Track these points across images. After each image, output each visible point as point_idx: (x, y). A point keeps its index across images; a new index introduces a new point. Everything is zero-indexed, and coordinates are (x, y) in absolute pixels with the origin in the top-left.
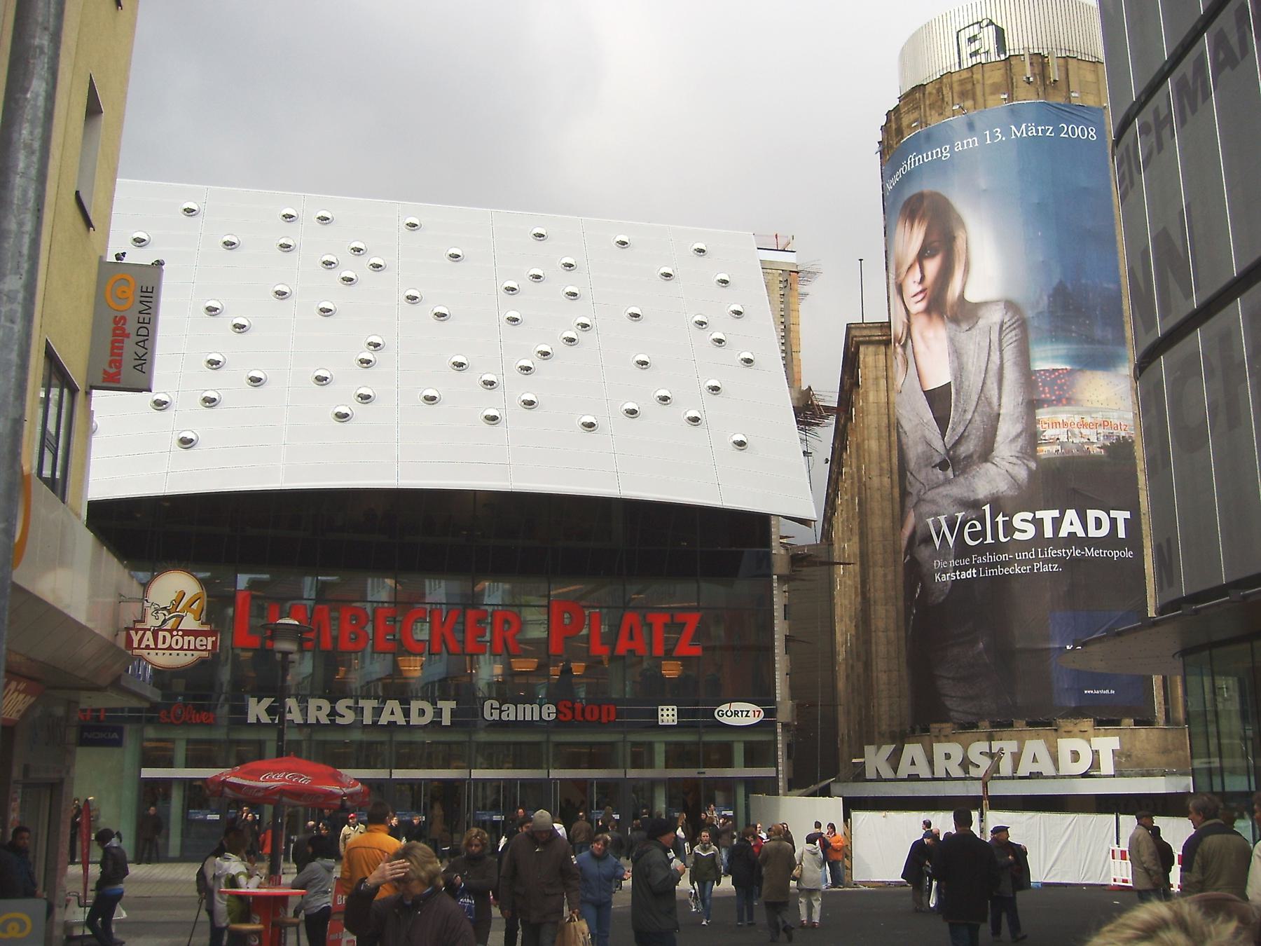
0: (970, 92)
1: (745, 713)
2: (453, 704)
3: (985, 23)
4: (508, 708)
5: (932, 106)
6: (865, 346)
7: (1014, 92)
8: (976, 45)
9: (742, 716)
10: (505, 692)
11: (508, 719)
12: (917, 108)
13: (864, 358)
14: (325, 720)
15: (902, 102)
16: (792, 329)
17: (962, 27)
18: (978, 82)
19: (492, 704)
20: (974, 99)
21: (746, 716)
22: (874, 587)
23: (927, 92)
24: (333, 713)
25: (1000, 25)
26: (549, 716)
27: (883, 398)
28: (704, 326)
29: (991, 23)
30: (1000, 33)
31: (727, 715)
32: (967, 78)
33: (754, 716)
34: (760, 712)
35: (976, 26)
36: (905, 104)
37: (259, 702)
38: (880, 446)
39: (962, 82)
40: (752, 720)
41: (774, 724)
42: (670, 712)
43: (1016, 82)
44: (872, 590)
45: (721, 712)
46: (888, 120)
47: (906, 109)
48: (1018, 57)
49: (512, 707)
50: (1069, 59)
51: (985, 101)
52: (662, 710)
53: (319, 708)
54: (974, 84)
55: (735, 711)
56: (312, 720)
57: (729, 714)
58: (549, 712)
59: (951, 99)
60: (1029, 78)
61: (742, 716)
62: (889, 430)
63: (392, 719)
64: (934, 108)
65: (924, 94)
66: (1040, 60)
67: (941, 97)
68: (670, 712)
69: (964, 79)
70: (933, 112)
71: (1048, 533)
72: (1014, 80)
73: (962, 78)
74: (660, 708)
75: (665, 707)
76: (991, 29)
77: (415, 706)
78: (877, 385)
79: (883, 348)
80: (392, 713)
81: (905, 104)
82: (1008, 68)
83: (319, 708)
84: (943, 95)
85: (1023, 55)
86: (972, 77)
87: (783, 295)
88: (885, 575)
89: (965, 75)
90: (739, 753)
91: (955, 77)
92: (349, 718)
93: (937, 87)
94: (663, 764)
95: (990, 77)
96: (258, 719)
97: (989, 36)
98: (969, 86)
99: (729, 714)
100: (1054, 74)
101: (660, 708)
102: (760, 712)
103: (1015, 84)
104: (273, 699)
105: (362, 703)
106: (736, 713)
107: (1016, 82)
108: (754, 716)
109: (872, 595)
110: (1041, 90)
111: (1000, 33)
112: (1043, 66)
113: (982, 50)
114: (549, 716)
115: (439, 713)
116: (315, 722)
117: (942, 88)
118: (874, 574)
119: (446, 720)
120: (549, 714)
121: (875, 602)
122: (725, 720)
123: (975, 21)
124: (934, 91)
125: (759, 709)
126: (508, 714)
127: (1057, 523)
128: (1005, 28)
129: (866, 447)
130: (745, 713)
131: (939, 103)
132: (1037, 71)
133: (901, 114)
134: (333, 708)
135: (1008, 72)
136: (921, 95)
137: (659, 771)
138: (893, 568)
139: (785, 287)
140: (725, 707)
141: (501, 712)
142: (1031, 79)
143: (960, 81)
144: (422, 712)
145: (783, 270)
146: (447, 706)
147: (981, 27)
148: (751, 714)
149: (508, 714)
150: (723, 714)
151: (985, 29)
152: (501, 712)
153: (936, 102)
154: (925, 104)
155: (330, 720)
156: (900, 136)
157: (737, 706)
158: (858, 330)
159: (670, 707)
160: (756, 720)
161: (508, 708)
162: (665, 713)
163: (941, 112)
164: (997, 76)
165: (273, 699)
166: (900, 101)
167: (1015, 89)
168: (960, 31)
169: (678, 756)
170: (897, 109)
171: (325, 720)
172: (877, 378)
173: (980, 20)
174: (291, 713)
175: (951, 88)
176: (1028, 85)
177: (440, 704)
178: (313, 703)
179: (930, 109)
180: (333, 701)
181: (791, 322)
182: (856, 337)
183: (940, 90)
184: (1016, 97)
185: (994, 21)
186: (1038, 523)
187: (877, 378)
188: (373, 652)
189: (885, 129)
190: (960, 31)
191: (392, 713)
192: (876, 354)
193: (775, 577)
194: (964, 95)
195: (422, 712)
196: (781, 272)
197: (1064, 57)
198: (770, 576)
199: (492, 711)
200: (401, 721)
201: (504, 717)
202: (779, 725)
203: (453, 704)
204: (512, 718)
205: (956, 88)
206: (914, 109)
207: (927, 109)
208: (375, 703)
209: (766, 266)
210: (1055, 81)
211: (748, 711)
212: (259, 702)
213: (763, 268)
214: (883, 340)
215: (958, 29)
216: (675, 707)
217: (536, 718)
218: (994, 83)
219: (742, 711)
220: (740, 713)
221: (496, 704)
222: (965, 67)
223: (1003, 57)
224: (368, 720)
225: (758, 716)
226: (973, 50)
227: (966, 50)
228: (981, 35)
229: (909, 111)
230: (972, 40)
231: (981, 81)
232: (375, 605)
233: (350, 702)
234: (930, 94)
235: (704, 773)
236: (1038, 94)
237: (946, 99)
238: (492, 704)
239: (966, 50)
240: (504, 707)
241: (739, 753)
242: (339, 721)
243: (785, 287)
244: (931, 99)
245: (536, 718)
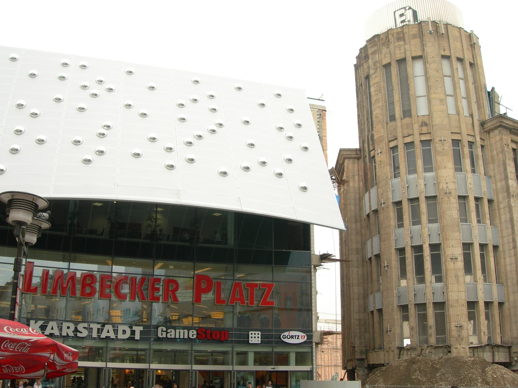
0: (402, 38)
1: (297, 337)
2: (141, 328)
3: (407, 8)
4: (171, 331)
5: (383, 44)
6: (348, 159)
7: (424, 38)
8: (403, 18)
9: (295, 338)
10: (168, 323)
11: (180, 330)
12: (376, 45)
13: (347, 165)
14: (71, 334)
15: (368, 43)
16: (323, 138)
17: (397, 10)
18: (406, 33)
19: (162, 329)
20: (404, 40)
21: (298, 338)
22: (352, 278)
23: (380, 38)
24: (76, 330)
25: (414, 9)
26: (193, 336)
27: (357, 185)
28: (282, 130)
29: (410, 8)
30: (415, 13)
31: (287, 338)
32: (401, 31)
33: (302, 338)
34: (305, 336)
35: (403, 9)
36: (370, 44)
37: (36, 323)
38: (355, 208)
39: (398, 33)
40: (301, 341)
41: (311, 343)
42: (257, 336)
43: (425, 33)
44: (351, 279)
45: (284, 336)
46: (360, 52)
47: (370, 46)
48: (425, 22)
49: (173, 331)
50: (448, 25)
51: (410, 42)
52: (258, 334)
53: (68, 328)
54: (404, 34)
55: (292, 336)
56: (64, 334)
57: (289, 337)
58: (193, 334)
59: (393, 40)
60: (431, 31)
61: (295, 338)
62: (360, 201)
63: (108, 335)
64: (384, 45)
65: (379, 39)
66: (435, 24)
67: (388, 40)
68: (257, 336)
69: (399, 32)
70: (384, 47)
71: (95, 335)
72: (424, 33)
73: (398, 31)
74: (250, 332)
75: (253, 332)
76: (411, 11)
77: (121, 328)
78: (354, 179)
79: (356, 160)
80: (108, 332)
81: (370, 44)
82: (420, 27)
83: (68, 328)
84: (389, 39)
85: (428, 21)
86: (403, 31)
87: (319, 121)
88: (358, 272)
89: (399, 30)
90: (292, 358)
91: (395, 31)
92: (85, 333)
93: (386, 35)
94: (409, 307)
95: (412, 31)
96: (67, 334)
97: (409, 15)
98: (401, 35)
99: (289, 337)
100: (443, 31)
101: (250, 332)
102: (305, 336)
103: (424, 34)
104: (44, 321)
105: (92, 326)
106: (292, 337)
107: (425, 33)
108: (302, 338)
109: (351, 281)
110: (436, 37)
111: (415, 13)
112: (436, 27)
113: (407, 20)
114: (193, 336)
115: (133, 332)
116: (66, 335)
117: (388, 35)
118: (352, 271)
119: (137, 337)
120: (193, 335)
121: (353, 285)
122: (286, 340)
123: (403, 7)
124: (384, 38)
125: (304, 335)
126: (171, 335)
127: (100, 331)
128: (417, 10)
129: (349, 208)
130: (297, 337)
131: (387, 43)
132: (434, 29)
133: (367, 48)
134: (76, 328)
135: (420, 29)
136: (378, 39)
137: (251, 367)
138: (362, 268)
139: (320, 117)
140: (286, 334)
141: (167, 333)
142: (432, 32)
143: (397, 32)
144: (124, 332)
145: (319, 109)
146: (138, 329)
147: (406, 10)
148: (300, 337)
149: (171, 335)
150: (285, 337)
151: (408, 11)
152: (167, 333)
153: (386, 42)
154: (380, 44)
155: (74, 334)
156: (367, 59)
157: (293, 333)
158: (345, 151)
159: (257, 333)
160: (303, 341)
161: (171, 331)
162: (253, 336)
163: (387, 47)
164: (415, 31)
165: (44, 321)
166: (367, 43)
167: (424, 37)
168: (396, 11)
169: (261, 359)
170: (366, 47)
171: (71, 334)
172: (354, 175)
173: (405, 7)
174: (53, 329)
175: (393, 36)
176: (430, 35)
177: (134, 328)
178: (65, 325)
179: (382, 46)
180: (76, 323)
181: (323, 135)
182: (343, 155)
183: (387, 37)
184: (425, 40)
185: (412, 7)
186: (90, 330)
187: (354, 175)
188: (80, 281)
189: (358, 58)
190: (396, 11)
191: (108, 332)
192: (354, 163)
193: (313, 266)
194: (399, 39)
195: (124, 332)
196: (318, 110)
197: (446, 24)
198: (310, 265)
199: (163, 332)
200: (112, 335)
201: (169, 336)
202: (314, 344)
203: (141, 328)
204: (173, 336)
205: (395, 36)
206: (375, 45)
207: (381, 46)
208: (99, 326)
209: (312, 107)
210: (443, 34)
211: (299, 336)
212: (36, 323)
213: (311, 108)
214: (357, 157)
215: (395, 11)
216: (260, 333)
217: (186, 337)
218: (413, 34)
219: (295, 336)
220: (294, 337)
221: (164, 329)
222: (399, 26)
223: (416, 23)
224: (95, 335)
225: (304, 339)
226: (402, 20)
227: (399, 20)
228: (406, 13)
229: (372, 47)
230: (402, 15)
231: (408, 33)
232: (101, 273)
233: (86, 325)
234: (382, 39)
235: (272, 368)
236: (435, 40)
237: (390, 41)
238: (162, 329)
239: (399, 20)
240: (169, 331)
241: (292, 358)
242: (79, 335)
243: (320, 117)
244: (383, 41)
245: (186, 337)
